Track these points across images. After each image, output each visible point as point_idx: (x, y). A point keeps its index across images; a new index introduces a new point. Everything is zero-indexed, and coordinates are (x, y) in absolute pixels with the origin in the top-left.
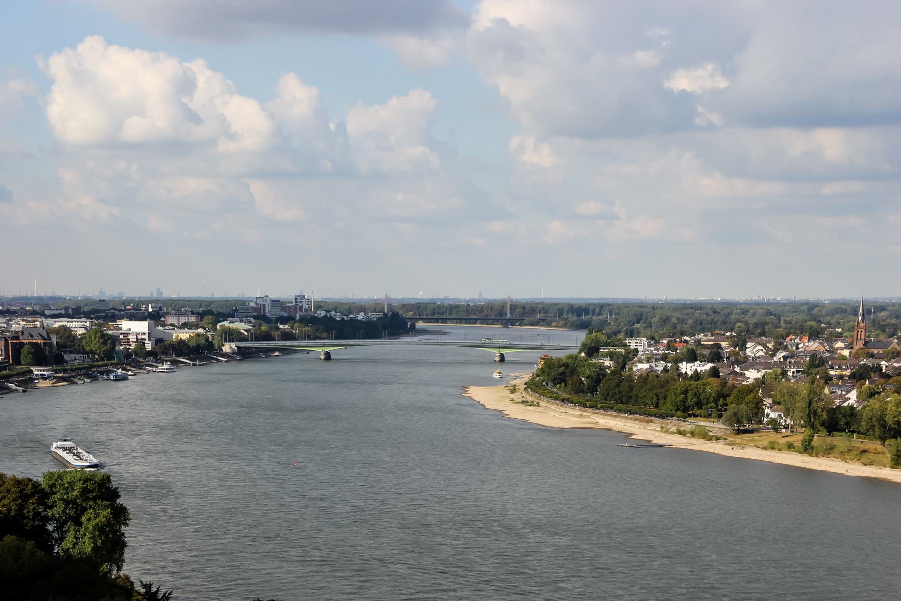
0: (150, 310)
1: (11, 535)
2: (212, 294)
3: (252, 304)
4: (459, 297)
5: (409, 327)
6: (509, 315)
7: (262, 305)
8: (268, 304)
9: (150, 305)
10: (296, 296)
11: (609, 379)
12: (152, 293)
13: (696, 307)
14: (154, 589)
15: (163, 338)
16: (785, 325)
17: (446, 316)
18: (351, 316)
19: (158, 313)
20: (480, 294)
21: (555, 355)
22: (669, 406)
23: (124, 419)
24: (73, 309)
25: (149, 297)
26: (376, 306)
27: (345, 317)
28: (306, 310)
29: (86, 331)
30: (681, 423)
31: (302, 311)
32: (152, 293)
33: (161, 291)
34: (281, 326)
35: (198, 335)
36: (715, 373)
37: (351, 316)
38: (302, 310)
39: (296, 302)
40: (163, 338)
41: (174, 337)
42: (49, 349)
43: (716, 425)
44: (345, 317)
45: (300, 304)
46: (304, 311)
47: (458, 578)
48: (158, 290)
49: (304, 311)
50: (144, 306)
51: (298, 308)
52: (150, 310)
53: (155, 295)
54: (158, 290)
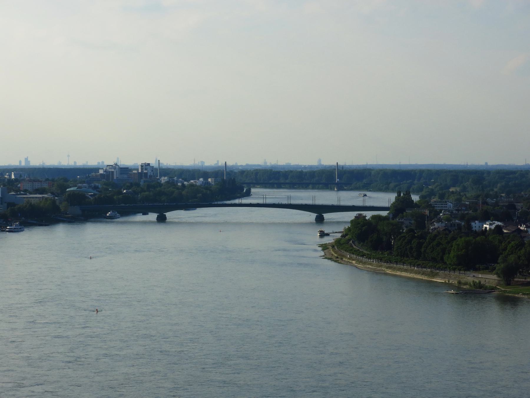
0: (13, 177)
2: (75, 162)
3: (101, 172)
4: (300, 164)
5: (245, 191)
7: (111, 173)
8: (117, 172)
9: (13, 173)
10: (142, 164)
11: (403, 237)
12: (20, 162)
17: (282, 181)
18: (192, 181)
20: (320, 160)
23: (430, 384)
25: (18, 166)
27: (185, 183)
28: (150, 176)
30: (462, 276)
31: (147, 177)
32: (20, 162)
33: (29, 160)
34: (157, 189)
35: (46, 199)
37: (192, 181)
38: (147, 176)
39: (142, 169)
41: (484, 183)
42: (111, 211)
44: (185, 183)
45: (145, 171)
46: (148, 177)
47: (81, 364)
48: (26, 159)
49: (148, 177)
50: (7, 174)
51: (143, 175)
54: (26, 159)
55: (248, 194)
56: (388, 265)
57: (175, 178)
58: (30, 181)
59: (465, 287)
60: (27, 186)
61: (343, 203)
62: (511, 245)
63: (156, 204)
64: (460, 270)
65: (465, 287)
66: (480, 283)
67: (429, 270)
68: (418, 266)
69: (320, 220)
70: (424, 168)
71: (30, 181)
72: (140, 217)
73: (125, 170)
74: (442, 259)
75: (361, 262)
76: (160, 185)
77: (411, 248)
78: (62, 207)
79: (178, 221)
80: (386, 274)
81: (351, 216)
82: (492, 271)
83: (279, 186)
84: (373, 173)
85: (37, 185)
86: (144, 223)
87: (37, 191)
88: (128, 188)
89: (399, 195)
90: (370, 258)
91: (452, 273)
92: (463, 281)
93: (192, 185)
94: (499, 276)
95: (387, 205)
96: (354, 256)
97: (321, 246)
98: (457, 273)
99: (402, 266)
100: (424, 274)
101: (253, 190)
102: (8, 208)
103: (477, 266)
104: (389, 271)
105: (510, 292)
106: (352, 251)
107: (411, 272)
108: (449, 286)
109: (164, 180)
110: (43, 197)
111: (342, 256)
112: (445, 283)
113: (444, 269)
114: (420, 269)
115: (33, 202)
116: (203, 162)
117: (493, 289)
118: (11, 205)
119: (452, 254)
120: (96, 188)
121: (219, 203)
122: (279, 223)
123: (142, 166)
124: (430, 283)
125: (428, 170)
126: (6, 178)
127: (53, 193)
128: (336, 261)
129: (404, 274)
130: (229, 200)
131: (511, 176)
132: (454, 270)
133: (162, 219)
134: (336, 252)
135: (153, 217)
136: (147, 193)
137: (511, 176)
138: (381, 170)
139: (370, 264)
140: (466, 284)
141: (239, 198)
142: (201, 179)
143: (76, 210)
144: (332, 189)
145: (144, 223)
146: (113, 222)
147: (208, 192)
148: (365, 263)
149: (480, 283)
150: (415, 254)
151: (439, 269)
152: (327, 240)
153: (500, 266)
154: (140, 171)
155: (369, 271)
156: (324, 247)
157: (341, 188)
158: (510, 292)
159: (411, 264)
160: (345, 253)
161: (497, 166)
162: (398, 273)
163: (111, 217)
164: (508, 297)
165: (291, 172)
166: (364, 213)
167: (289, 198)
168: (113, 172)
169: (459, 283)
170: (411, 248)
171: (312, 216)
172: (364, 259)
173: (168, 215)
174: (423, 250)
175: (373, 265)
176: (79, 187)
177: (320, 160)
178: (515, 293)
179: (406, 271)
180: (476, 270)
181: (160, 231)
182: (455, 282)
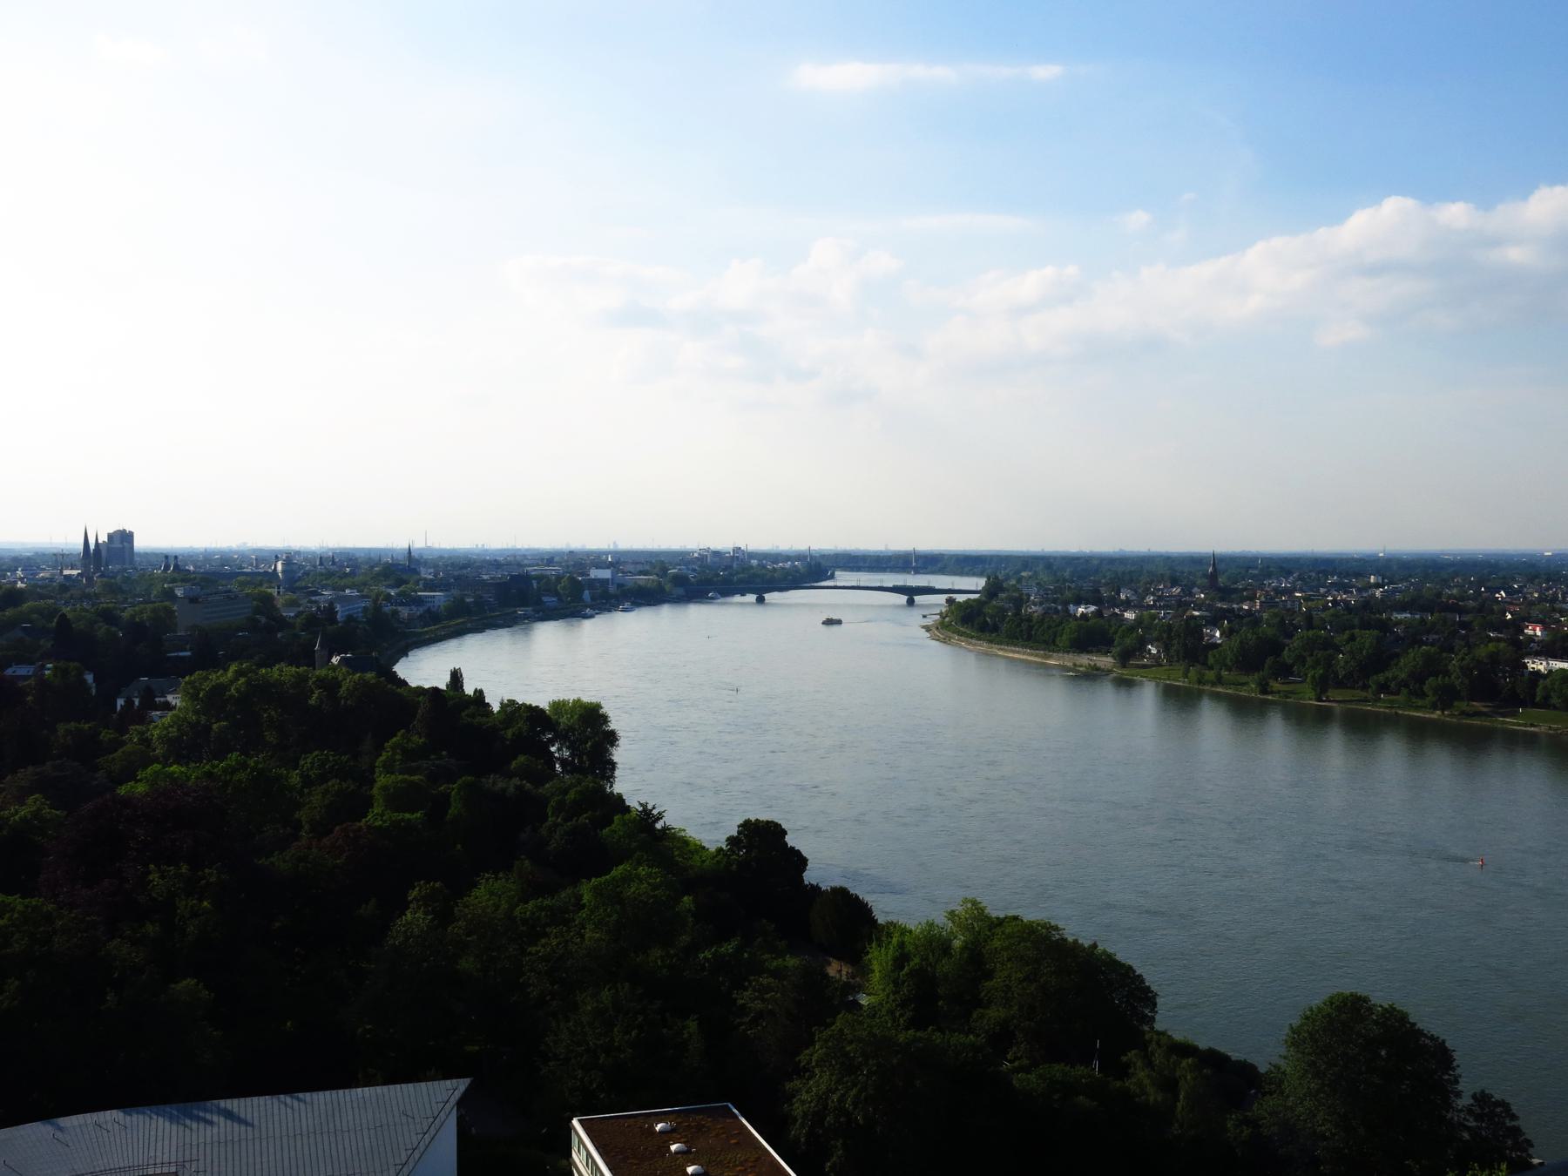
0: (610, 560)
1: (596, 877)
3: (696, 555)
6: (914, 564)
12: (609, 546)
13: (682, 557)
14: (650, 807)
15: (125, 537)
16: (1145, 571)
17: (861, 564)
19: (617, 563)
20: (887, 545)
21: (960, 598)
22: (1063, 640)
24: (547, 559)
26: (800, 557)
29: (1376, 632)
30: (1076, 658)
32: (609, 546)
35: (653, 580)
36: (1098, 614)
40: (125, 537)
43: (1104, 659)
48: (615, 543)
52: (610, 560)
53: (612, 547)
54: (615, 543)
55: (832, 577)
56: (999, 647)
57: (764, 562)
58: (633, 563)
59: (1081, 669)
60: (630, 568)
61: (956, 588)
62: (1121, 629)
63: (752, 586)
64: (1074, 653)
65: (1081, 669)
66: (1095, 665)
67: (1042, 652)
68: (1031, 648)
69: (911, 602)
70: (826, 553)
71: (633, 563)
72: (738, 598)
73: (716, 554)
74: (1054, 641)
75: (970, 644)
76: (752, 567)
77: (1022, 631)
78: (668, 587)
79: (540, 572)
80: (997, 656)
81: (942, 599)
82: (1106, 653)
83: (859, 569)
84: (556, 559)
85: (640, 567)
86: (742, 604)
87: (641, 573)
88: (723, 570)
89: (989, 578)
90: (980, 640)
91: (1066, 655)
92: (1078, 663)
93: (782, 568)
94: (1115, 659)
95: (980, 588)
96: (963, 638)
97: (923, 627)
98: (1071, 656)
99: (1013, 649)
100: (1037, 656)
101: (837, 573)
102: (618, 588)
103: (1090, 649)
104: (1000, 653)
105: (1127, 674)
106: (961, 634)
107: (1024, 653)
108: (1064, 668)
109: (754, 562)
110: (649, 579)
111: (950, 638)
112: (1060, 665)
113: (1058, 651)
114: (1032, 651)
115: (641, 583)
116: (778, 547)
117: (1110, 671)
118: (620, 586)
119: (1064, 637)
120: (694, 570)
121: (809, 585)
122: (867, 606)
123: (734, 550)
124: (1048, 667)
125: (998, 556)
126: (1370, 578)
127: (658, 575)
128: (945, 642)
129: (1016, 656)
130: (817, 582)
131: (1076, 562)
132: (1068, 652)
133: (761, 600)
134: (943, 634)
135: (752, 598)
136: (742, 575)
137: (1076, 562)
138: (954, 555)
139: (980, 646)
140: (1081, 666)
141: (825, 580)
142: (789, 563)
143: (680, 591)
144: (909, 573)
145: (742, 604)
146: (732, 604)
147: (798, 574)
148: (975, 645)
149: (1095, 665)
150: (1025, 637)
151: (1054, 651)
152: (929, 622)
153: (1115, 650)
154: (732, 554)
155: (979, 653)
156: (927, 629)
157: (917, 571)
158: (1127, 674)
159: (1023, 646)
160: (952, 635)
161: (1064, 552)
162: (1011, 655)
163: (712, 598)
164: (1126, 679)
165: (870, 556)
166: (954, 596)
167: (882, 581)
168: (706, 556)
169: (1075, 665)
170: (1022, 631)
171: (903, 599)
172: (974, 641)
173: (767, 596)
174: (1033, 633)
175: (984, 646)
176: (680, 569)
177: (887, 545)
178: (1133, 675)
179: (1018, 652)
180: (1089, 652)
181: (760, 609)
182: (1070, 664)
